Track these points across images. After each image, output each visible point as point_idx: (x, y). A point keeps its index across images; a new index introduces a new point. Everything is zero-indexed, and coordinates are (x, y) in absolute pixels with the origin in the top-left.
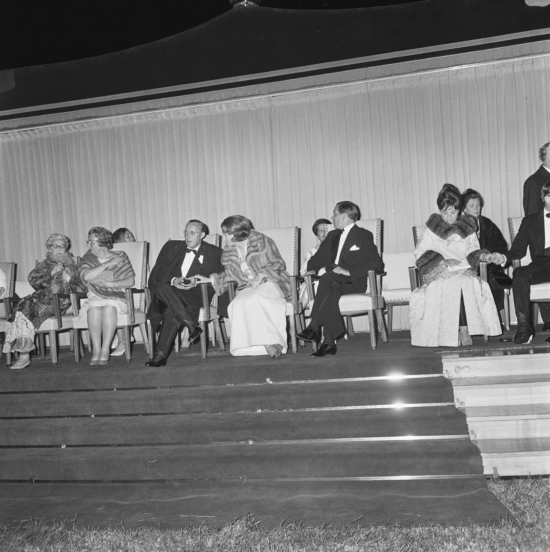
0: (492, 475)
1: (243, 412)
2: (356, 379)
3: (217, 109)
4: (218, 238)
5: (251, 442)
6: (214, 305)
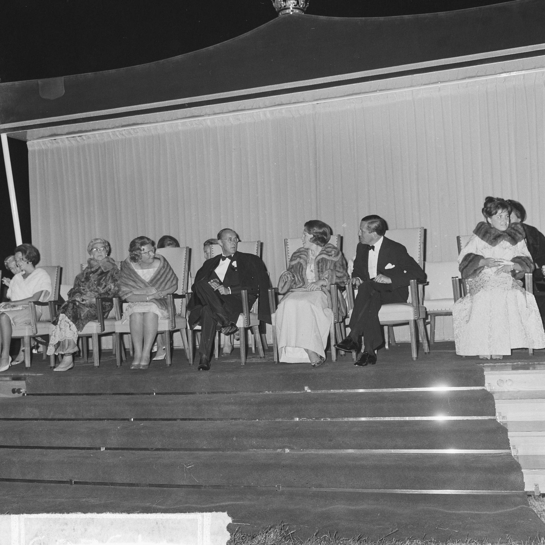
0: (533, 492)
1: (280, 420)
2: (395, 390)
3: (261, 115)
4: (259, 244)
5: (287, 451)
6: (255, 312)
